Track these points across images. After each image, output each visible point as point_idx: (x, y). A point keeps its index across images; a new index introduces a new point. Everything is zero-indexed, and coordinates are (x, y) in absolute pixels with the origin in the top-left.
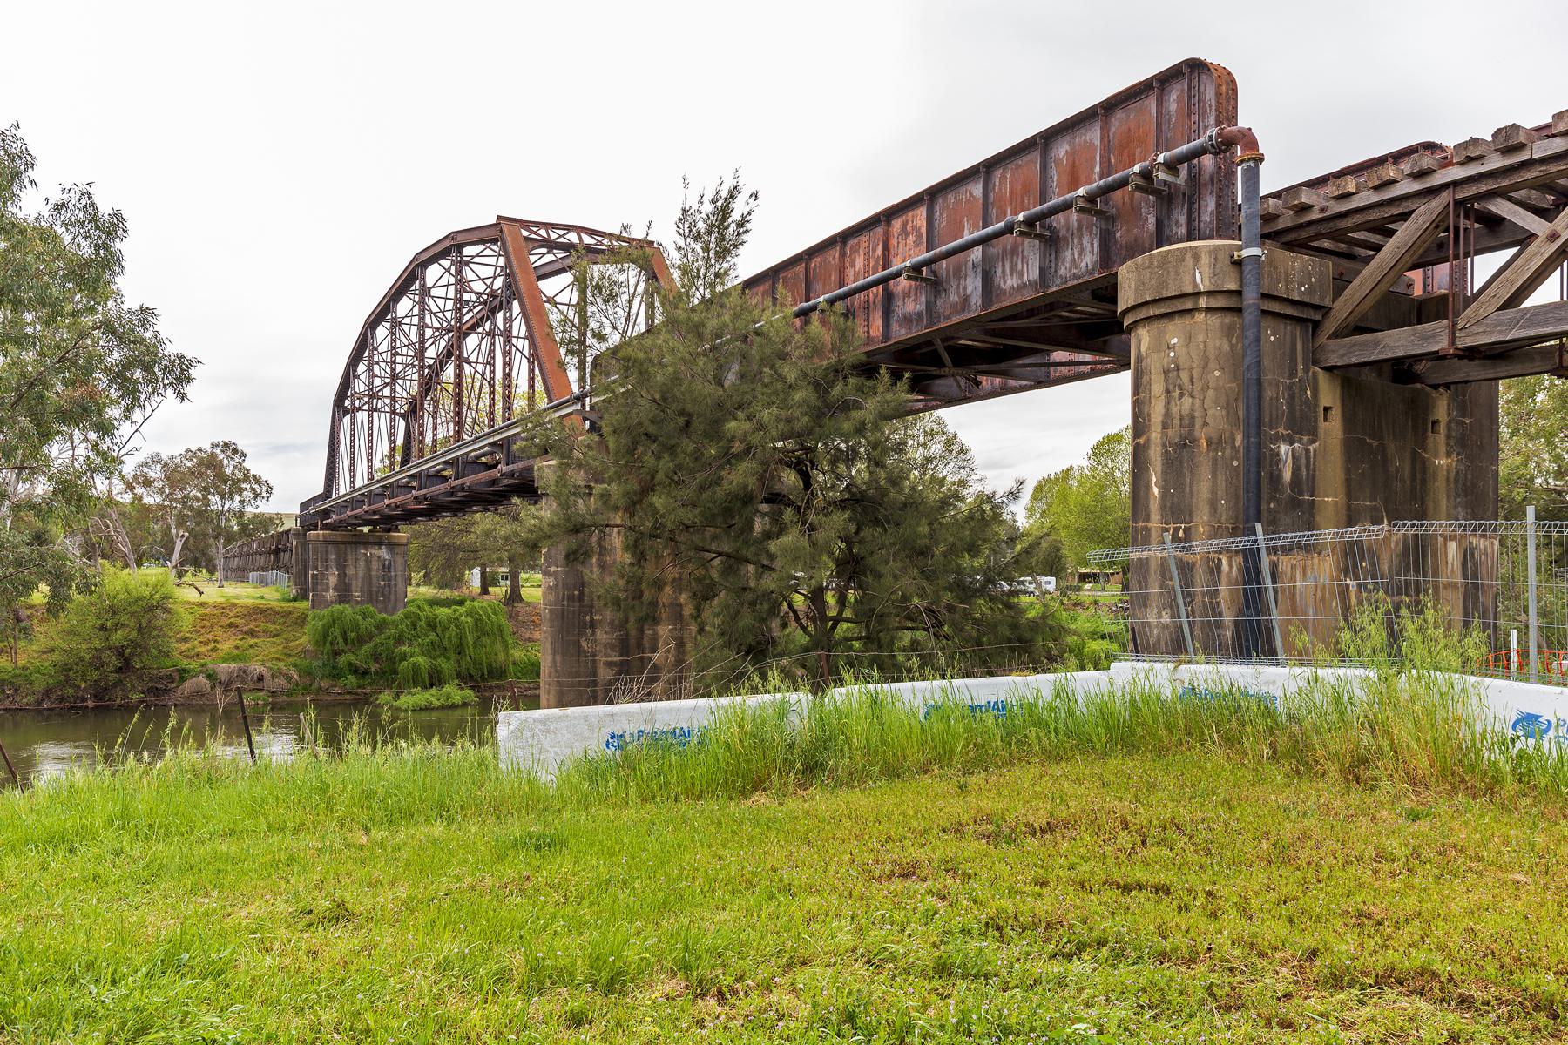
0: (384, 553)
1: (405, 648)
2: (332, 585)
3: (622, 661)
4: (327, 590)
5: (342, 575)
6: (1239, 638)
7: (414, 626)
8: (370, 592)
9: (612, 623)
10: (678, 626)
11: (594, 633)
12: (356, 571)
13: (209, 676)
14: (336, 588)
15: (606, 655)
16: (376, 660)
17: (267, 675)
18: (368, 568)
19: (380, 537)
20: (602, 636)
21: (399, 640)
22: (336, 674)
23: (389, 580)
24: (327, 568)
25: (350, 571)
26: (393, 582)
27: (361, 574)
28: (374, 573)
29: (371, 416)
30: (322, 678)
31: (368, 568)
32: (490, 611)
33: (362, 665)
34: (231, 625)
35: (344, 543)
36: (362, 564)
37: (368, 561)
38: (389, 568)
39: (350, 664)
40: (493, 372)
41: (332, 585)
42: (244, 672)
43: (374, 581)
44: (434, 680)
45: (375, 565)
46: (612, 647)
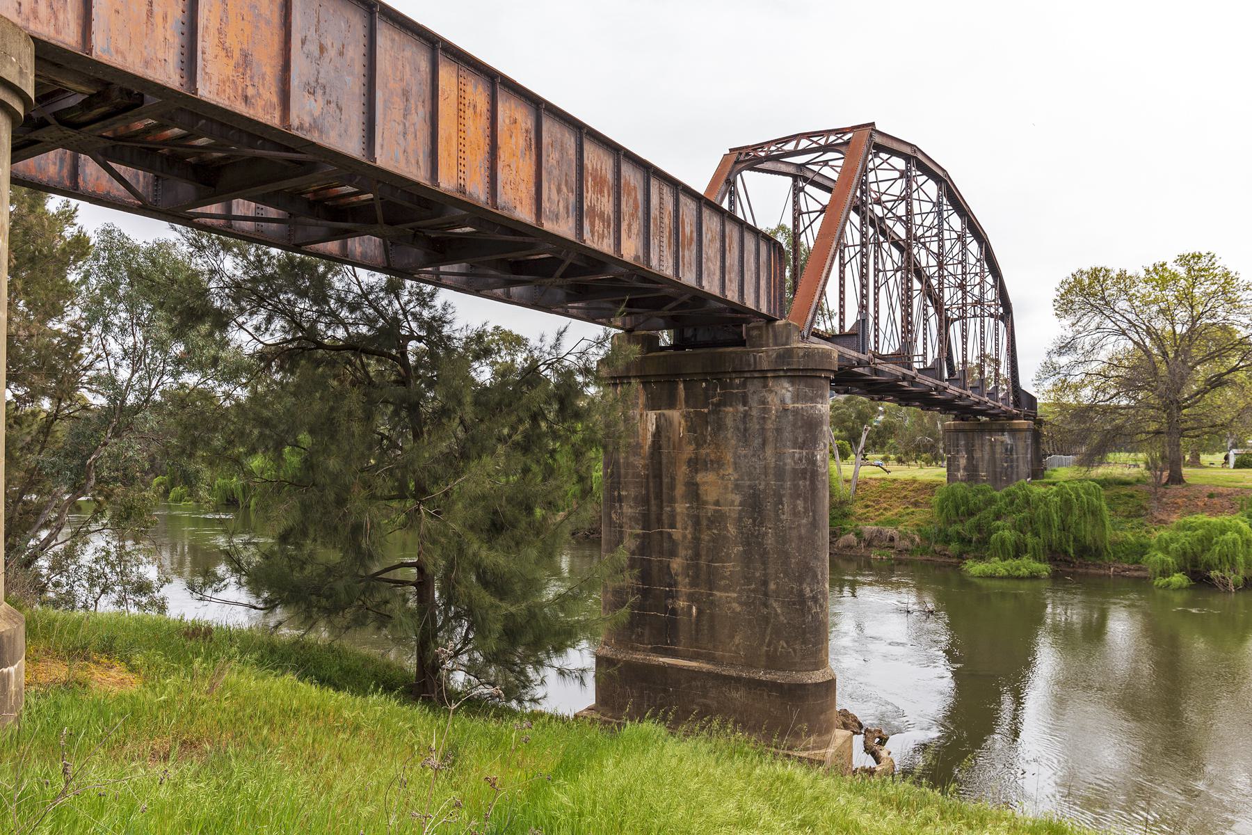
0: (1006, 438)
1: (999, 523)
2: (962, 466)
3: (644, 534)
4: (958, 470)
5: (970, 458)
7: (1012, 502)
8: (995, 472)
9: (636, 497)
10: (695, 505)
11: (621, 507)
12: (982, 454)
13: (857, 535)
14: (965, 469)
15: (631, 527)
16: (980, 531)
17: (897, 538)
18: (993, 452)
19: (1003, 424)
20: (628, 510)
21: (998, 517)
22: (947, 540)
24: (958, 452)
25: (977, 455)
26: (1015, 464)
27: (986, 457)
28: (998, 456)
29: (982, 322)
30: (936, 542)
31: (993, 452)
32: (1081, 492)
33: (967, 535)
34: (905, 497)
35: (972, 431)
36: (987, 448)
37: (992, 445)
39: (958, 533)
40: (876, 263)
41: (962, 466)
42: (881, 533)
43: (998, 462)
44: (1019, 551)
45: (998, 449)
46: (636, 520)
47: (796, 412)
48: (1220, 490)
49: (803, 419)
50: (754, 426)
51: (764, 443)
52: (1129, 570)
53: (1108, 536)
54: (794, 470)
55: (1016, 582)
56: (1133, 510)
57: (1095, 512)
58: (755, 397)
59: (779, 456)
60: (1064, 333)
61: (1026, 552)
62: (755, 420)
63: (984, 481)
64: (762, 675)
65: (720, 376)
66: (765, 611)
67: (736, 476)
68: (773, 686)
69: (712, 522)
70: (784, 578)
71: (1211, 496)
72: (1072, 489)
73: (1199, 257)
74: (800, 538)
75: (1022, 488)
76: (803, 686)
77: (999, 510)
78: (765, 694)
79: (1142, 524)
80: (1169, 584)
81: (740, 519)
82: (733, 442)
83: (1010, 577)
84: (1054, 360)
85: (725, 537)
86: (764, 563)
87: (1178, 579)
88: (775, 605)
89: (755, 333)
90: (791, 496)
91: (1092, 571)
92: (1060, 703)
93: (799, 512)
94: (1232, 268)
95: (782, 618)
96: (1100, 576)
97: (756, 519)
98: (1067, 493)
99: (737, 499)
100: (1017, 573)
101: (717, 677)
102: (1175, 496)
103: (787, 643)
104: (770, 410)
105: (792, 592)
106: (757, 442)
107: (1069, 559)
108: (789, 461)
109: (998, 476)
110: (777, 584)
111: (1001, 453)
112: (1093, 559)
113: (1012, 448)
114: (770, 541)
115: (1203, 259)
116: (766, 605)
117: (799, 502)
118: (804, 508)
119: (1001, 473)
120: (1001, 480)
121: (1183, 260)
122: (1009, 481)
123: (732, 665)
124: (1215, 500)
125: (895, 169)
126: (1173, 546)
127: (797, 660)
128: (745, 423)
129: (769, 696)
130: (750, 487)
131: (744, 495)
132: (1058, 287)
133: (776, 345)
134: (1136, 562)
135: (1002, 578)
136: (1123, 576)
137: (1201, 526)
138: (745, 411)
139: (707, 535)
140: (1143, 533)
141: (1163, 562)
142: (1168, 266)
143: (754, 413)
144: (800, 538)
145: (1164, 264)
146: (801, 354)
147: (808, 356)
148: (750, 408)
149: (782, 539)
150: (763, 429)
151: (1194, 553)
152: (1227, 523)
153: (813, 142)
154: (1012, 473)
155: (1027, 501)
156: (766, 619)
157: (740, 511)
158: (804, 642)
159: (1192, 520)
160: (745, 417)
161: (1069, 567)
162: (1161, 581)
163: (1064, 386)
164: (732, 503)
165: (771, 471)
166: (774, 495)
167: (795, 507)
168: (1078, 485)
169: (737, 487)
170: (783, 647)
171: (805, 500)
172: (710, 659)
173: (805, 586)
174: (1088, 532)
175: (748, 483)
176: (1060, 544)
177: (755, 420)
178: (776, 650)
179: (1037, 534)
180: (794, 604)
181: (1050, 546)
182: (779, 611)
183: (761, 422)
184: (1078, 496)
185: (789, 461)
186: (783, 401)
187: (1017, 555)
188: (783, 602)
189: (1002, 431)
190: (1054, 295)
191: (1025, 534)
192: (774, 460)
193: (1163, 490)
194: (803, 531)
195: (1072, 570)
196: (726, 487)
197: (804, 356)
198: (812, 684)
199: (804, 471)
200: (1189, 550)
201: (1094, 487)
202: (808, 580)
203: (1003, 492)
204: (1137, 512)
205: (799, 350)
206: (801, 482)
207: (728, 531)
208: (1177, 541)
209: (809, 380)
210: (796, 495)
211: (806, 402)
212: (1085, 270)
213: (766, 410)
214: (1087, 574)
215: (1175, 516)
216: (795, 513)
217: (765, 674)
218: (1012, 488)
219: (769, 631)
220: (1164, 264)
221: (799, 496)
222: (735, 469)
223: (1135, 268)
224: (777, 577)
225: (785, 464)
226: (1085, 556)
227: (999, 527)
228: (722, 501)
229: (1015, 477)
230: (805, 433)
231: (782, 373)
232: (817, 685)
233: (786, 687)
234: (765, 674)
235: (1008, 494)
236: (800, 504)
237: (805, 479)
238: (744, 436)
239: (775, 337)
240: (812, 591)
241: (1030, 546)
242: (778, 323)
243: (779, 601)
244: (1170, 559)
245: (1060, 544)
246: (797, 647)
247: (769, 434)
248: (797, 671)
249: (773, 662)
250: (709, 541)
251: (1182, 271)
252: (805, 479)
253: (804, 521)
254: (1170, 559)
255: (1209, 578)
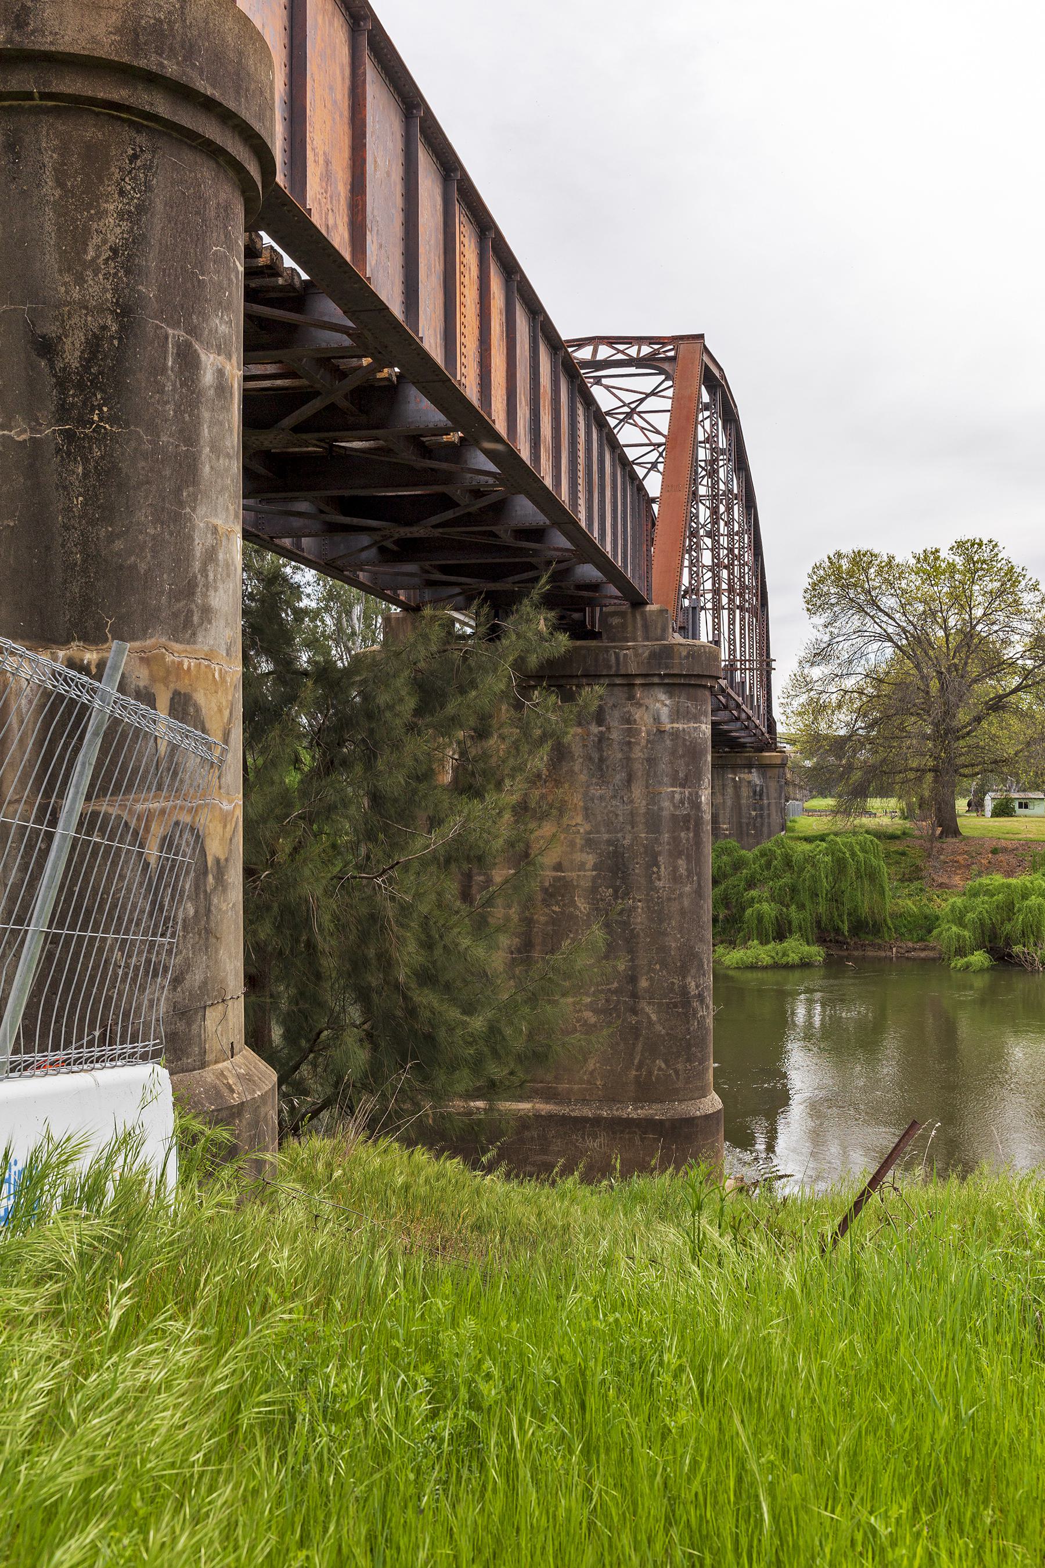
0: (755, 777)
1: (753, 893)
6: (62, 1539)
16: (727, 906)
18: (737, 796)
21: (751, 884)
23: (762, 809)
27: (729, 803)
28: (744, 801)
31: (737, 796)
32: (857, 848)
36: (730, 790)
37: (737, 787)
38: (761, 795)
43: (744, 810)
45: (745, 792)
47: (675, 735)
48: (1003, 843)
49: (684, 745)
50: (615, 755)
51: (629, 780)
52: (915, 949)
53: (887, 907)
54: (674, 817)
55: (784, 973)
56: (907, 871)
57: (873, 876)
58: (616, 714)
59: (653, 797)
60: (819, 636)
61: (791, 932)
62: (616, 746)
63: (726, 836)
64: (630, 1111)
65: (562, 682)
66: (633, 1019)
67: (588, 827)
68: (649, 1125)
69: (552, 895)
70: (661, 970)
71: (995, 851)
72: (845, 844)
73: (980, 545)
74: (683, 912)
75: (780, 844)
76: (689, 1122)
77: (753, 877)
78: (637, 1138)
79: (921, 890)
80: (967, 966)
81: (594, 889)
82: (583, 778)
83: (776, 966)
84: (806, 671)
85: (572, 917)
86: (631, 951)
87: (979, 958)
88: (648, 1009)
89: (615, 621)
90: (670, 854)
91: (871, 953)
92: (817, 1137)
93: (681, 876)
94: (1017, 562)
95: (659, 1028)
96: (880, 959)
97: (620, 887)
98: (840, 851)
99: (590, 859)
100: (784, 960)
101: (564, 1120)
102: (953, 853)
103: (666, 1062)
104: (638, 732)
105: (672, 990)
106: (619, 777)
107: (841, 938)
108: (666, 804)
109: (745, 829)
110: (651, 979)
111: (748, 797)
112: (871, 937)
113: (762, 790)
114: (640, 919)
115: (984, 547)
116: (634, 1011)
117: (680, 862)
118: (687, 870)
119: (748, 824)
120: (748, 834)
121: (960, 546)
122: (758, 839)
123: (585, 1101)
124: (1001, 857)
125: (607, 387)
126: (970, 916)
127: (680, 1085)
128: (600, 750)
129: (642, 1139)
130: (609, 842)
131: (600, 855)
132: (810, 572)
133: (647, 639)
134: (922, 940)
135: (765, 968)
136: (908, 958)
137: (999, 890)
138: (601, 732)
139: (546, 915)
140: (925, 901)
141: (959, 936)
142: (943, 554)
143: (615, 735)
144: (683, 912)
145: (937, 551)
146: (684, 653)
147: (693, 656)
148: (608, 729)
149: (658, 915)
150: (628, 759)
151: (993, 924)
152: (1029, 885)
153: (619, 351)
154: (762, 824)
155: (788, 863)
156: (635, 1031)
157: (594, 878)
158: (689, 1060)
159: (988, 882)
160: (600, 741)
161: (841, 949)
162: (960, 962)
163: (817, 709)
164: (582, 866)
165: (640, 819)
166: (646, 852)
167: (675, 869)
168: (852, 840)
169: (590, 843)
170: (660, 1069)
171: (689, 861)
172: (549, 1095)
173: (689, 979)
174: (865, 903)
175: (606, 836)
176: (831, 920)
177: (616, 746)
178: (650, 1073)
179: (801, 907)
180: (676, 1006)
181: (818, 923)
182: (654, 1017)
183: (625, 748)
184: (853, 854)
185: (666, 804)
186: (657, 719)
187: (780, 937)
188: (660, 1005)
189: (749, 766)
190: (805, 582)
191: (788, 906)
192: (644, 802)
193: (938, 845)
194: (686, 903)
195: (845, 953)
196: (572, 844)
197: (687, 657)
198: (701, 1117)
199: (686, 819)
200: (988, 921)
201: (871, 841)
202: (693, 971)
203: (756, 851)
204: (913, 875)
205: (682, 648)
206: (683, 834)
207: (576, 907)
208: (973, 909)
209: (691, 690)
210: (676, 852)
211: (689, 721)
212: (843, 551)
213: (631, 732)
214: (864, 958)
215: (957, 878)
216: (675, 878)
217: (636, 1109)
218: (768, 844)
219: (639, 1047)
220: (937, 551)
221: (680, 854)
222: (587, 817)
223: (904, 556)
224: (651, 970)
225: (661, 809)
226: (862, 936)
227: (753, 899)
228: (565, 864)
229: (765, 830)
230: (687, 765)
231: (656, 680)
232: (707, 1117)
233: (667, 1124)
234: (636, 1109)
235: (763, 854)
236: (682, 863)
237: (688, 829)
238: (600, 768)
239: (646, 627)
240: (697, 987)
241: (795, 923)
242: (648, 608)
243: (654, 1004)
244: (966, 933)
245: (831, 920)
246: (680, 1066)
247: (637, 766)
248: (680, 1101)
249: (646, 1092)
250: (546, 924)
251: (959, 561)
252: (688, 829)
253: (687, 889)
254: (966, 933)
255: (1010, 956)
